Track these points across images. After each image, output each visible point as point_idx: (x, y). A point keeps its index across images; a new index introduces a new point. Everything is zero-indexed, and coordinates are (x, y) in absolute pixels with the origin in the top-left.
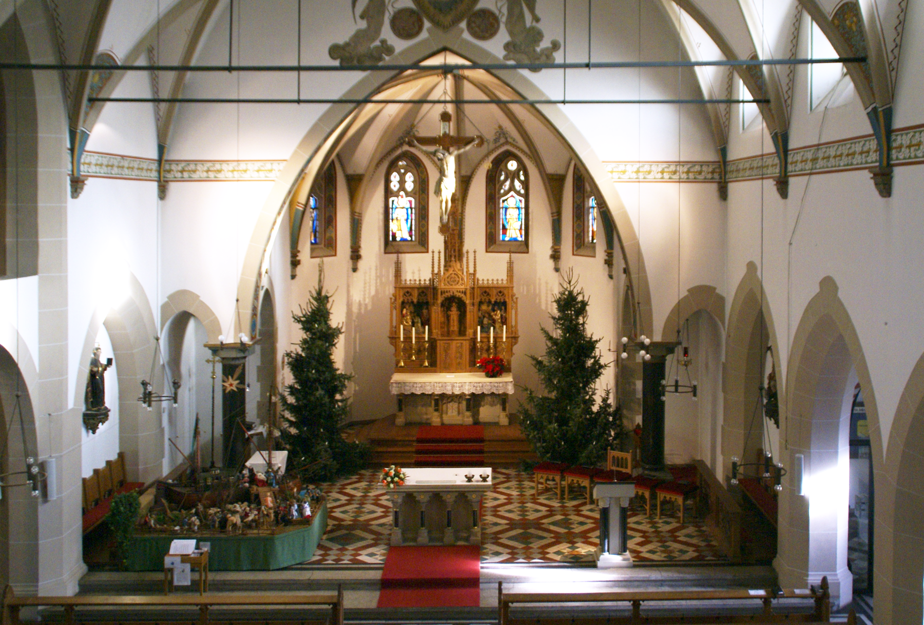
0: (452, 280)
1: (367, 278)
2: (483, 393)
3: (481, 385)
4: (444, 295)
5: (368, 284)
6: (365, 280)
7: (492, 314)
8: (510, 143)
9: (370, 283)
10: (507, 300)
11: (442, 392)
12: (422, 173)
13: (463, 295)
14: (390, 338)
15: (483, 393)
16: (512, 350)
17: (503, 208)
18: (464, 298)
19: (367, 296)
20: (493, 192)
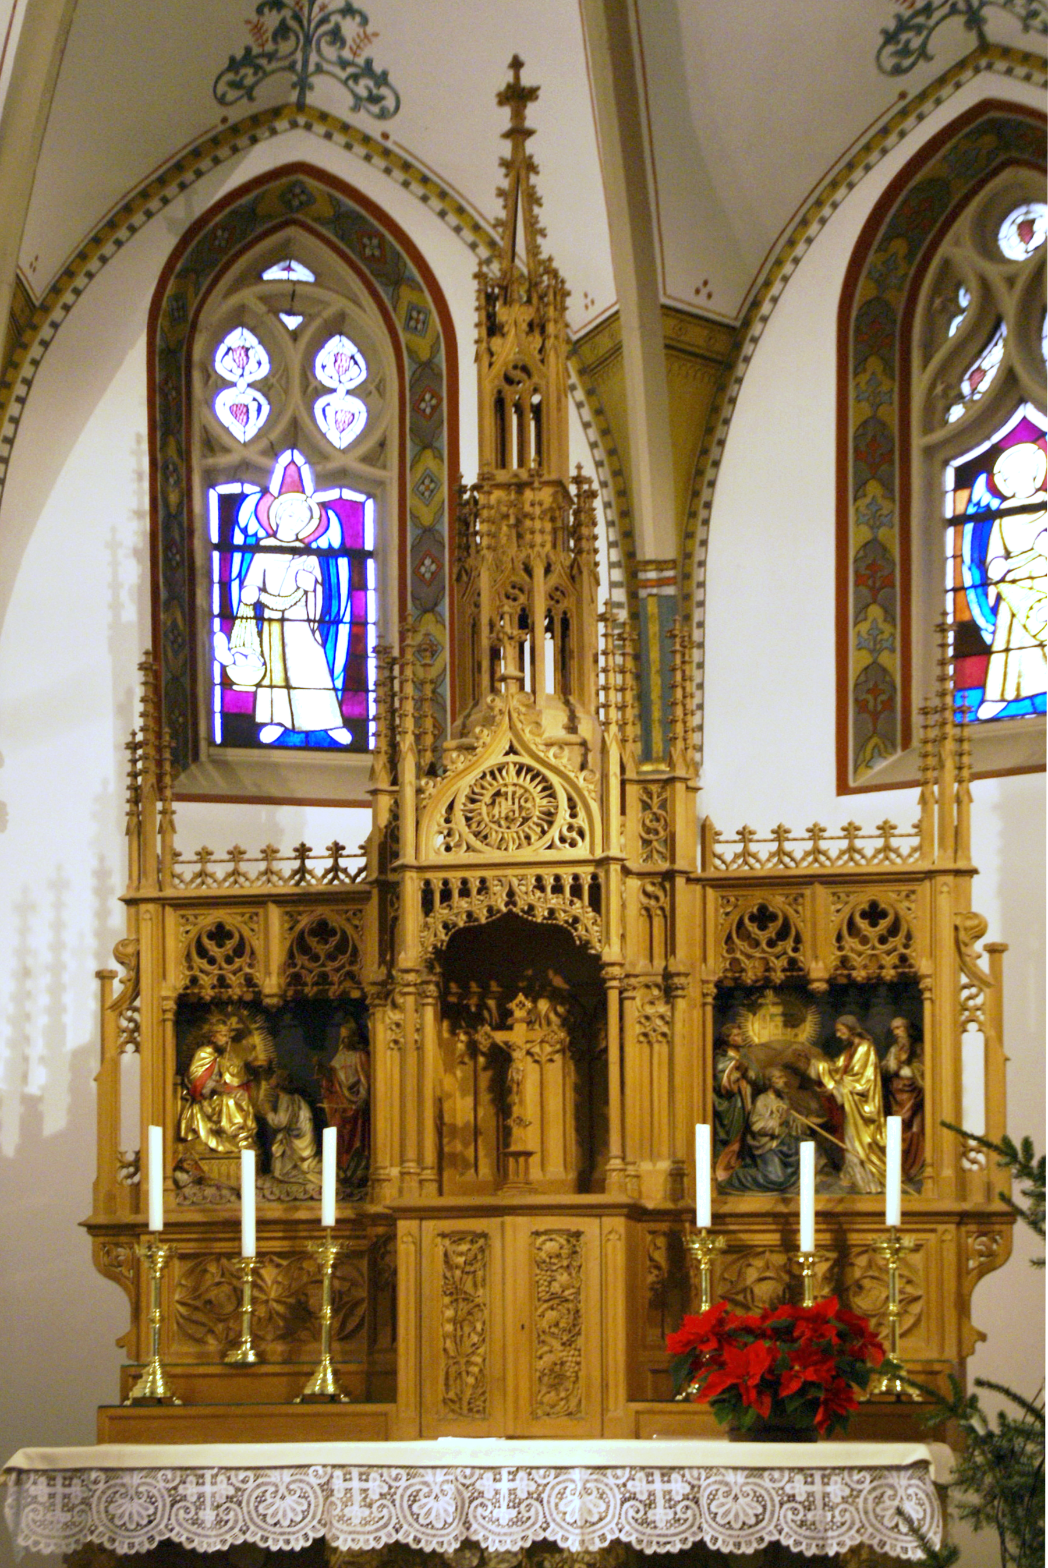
0: (504, 807)
1: (41, 939)
2: (700, 1545)
3: (678, 1487)
4: (441, 912)
5: (44, 980)
6: (23, 952)
7: (821, 1067)
8: (1006, 52)
9: (57, 968)
10: (923, 966)
11: (387, 1537)
12: (415, 319)
13: (580, 908)
14: (92, 1228)
15: (700, 1545)
16: (963, 1307)
17: (958, 521)
18: (588, 928)
19: (38, 1048)
20: (891, 416)
